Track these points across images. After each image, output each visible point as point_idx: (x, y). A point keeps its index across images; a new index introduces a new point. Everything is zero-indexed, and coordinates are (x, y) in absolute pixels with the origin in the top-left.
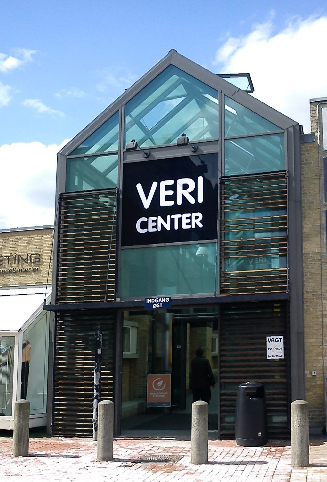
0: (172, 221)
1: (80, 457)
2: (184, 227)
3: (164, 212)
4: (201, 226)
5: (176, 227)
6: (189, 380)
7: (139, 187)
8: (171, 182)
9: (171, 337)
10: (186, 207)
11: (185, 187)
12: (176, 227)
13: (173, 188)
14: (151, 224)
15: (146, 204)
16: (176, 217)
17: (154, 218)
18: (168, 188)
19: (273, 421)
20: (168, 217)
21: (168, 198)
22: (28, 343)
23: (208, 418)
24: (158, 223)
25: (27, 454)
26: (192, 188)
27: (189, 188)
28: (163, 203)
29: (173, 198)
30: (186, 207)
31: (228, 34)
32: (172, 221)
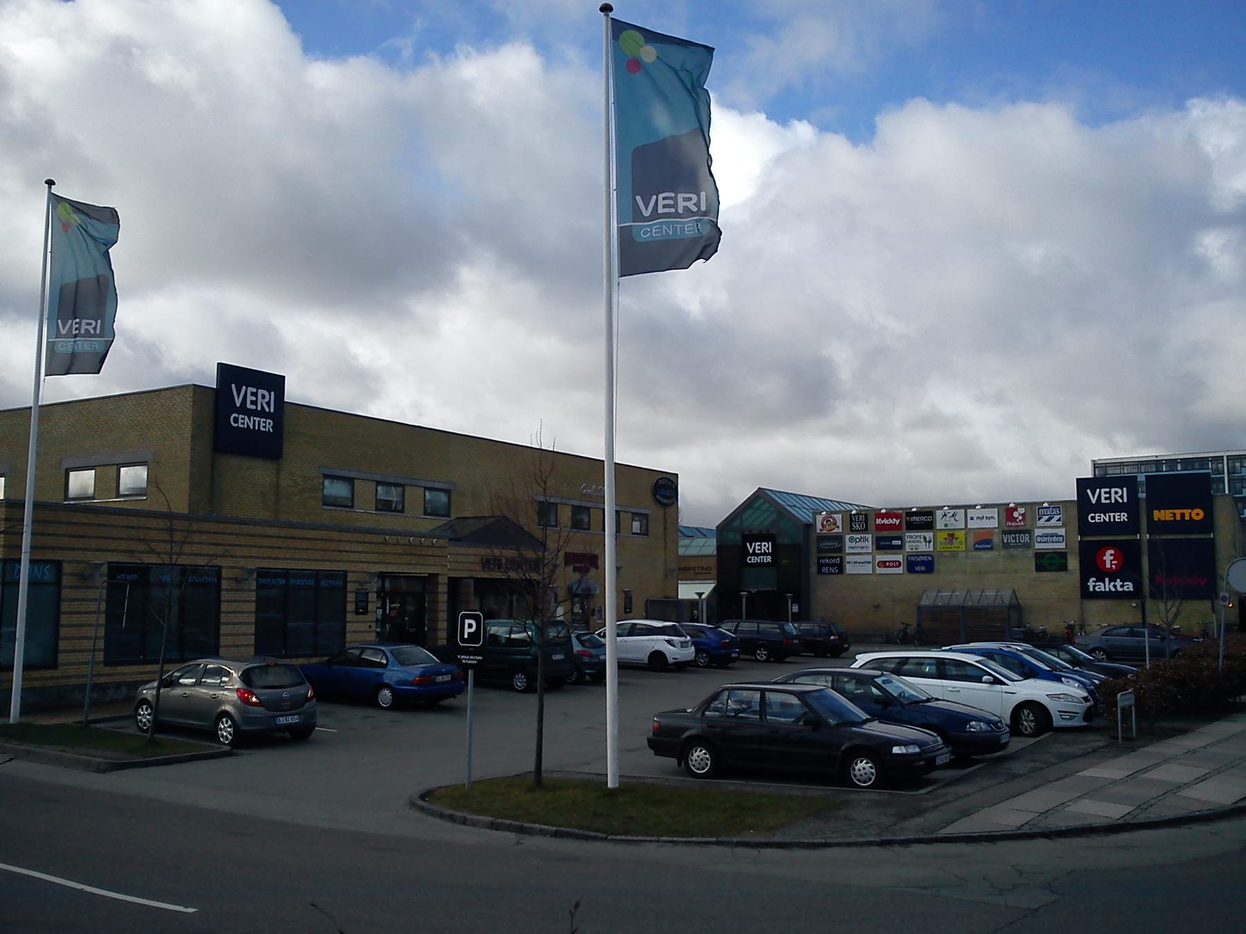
3: (758, 555)
8: (254, 390)
10: (765, 554)
11: (263, 397)
13: (1109, 493)
16: (257, 419)
18: (253, 394)
21: (252, 402)
24: (754, 560)
27: (766, 546)
28: (249, 406)
29: (1109, 498)
30: (765, 554)
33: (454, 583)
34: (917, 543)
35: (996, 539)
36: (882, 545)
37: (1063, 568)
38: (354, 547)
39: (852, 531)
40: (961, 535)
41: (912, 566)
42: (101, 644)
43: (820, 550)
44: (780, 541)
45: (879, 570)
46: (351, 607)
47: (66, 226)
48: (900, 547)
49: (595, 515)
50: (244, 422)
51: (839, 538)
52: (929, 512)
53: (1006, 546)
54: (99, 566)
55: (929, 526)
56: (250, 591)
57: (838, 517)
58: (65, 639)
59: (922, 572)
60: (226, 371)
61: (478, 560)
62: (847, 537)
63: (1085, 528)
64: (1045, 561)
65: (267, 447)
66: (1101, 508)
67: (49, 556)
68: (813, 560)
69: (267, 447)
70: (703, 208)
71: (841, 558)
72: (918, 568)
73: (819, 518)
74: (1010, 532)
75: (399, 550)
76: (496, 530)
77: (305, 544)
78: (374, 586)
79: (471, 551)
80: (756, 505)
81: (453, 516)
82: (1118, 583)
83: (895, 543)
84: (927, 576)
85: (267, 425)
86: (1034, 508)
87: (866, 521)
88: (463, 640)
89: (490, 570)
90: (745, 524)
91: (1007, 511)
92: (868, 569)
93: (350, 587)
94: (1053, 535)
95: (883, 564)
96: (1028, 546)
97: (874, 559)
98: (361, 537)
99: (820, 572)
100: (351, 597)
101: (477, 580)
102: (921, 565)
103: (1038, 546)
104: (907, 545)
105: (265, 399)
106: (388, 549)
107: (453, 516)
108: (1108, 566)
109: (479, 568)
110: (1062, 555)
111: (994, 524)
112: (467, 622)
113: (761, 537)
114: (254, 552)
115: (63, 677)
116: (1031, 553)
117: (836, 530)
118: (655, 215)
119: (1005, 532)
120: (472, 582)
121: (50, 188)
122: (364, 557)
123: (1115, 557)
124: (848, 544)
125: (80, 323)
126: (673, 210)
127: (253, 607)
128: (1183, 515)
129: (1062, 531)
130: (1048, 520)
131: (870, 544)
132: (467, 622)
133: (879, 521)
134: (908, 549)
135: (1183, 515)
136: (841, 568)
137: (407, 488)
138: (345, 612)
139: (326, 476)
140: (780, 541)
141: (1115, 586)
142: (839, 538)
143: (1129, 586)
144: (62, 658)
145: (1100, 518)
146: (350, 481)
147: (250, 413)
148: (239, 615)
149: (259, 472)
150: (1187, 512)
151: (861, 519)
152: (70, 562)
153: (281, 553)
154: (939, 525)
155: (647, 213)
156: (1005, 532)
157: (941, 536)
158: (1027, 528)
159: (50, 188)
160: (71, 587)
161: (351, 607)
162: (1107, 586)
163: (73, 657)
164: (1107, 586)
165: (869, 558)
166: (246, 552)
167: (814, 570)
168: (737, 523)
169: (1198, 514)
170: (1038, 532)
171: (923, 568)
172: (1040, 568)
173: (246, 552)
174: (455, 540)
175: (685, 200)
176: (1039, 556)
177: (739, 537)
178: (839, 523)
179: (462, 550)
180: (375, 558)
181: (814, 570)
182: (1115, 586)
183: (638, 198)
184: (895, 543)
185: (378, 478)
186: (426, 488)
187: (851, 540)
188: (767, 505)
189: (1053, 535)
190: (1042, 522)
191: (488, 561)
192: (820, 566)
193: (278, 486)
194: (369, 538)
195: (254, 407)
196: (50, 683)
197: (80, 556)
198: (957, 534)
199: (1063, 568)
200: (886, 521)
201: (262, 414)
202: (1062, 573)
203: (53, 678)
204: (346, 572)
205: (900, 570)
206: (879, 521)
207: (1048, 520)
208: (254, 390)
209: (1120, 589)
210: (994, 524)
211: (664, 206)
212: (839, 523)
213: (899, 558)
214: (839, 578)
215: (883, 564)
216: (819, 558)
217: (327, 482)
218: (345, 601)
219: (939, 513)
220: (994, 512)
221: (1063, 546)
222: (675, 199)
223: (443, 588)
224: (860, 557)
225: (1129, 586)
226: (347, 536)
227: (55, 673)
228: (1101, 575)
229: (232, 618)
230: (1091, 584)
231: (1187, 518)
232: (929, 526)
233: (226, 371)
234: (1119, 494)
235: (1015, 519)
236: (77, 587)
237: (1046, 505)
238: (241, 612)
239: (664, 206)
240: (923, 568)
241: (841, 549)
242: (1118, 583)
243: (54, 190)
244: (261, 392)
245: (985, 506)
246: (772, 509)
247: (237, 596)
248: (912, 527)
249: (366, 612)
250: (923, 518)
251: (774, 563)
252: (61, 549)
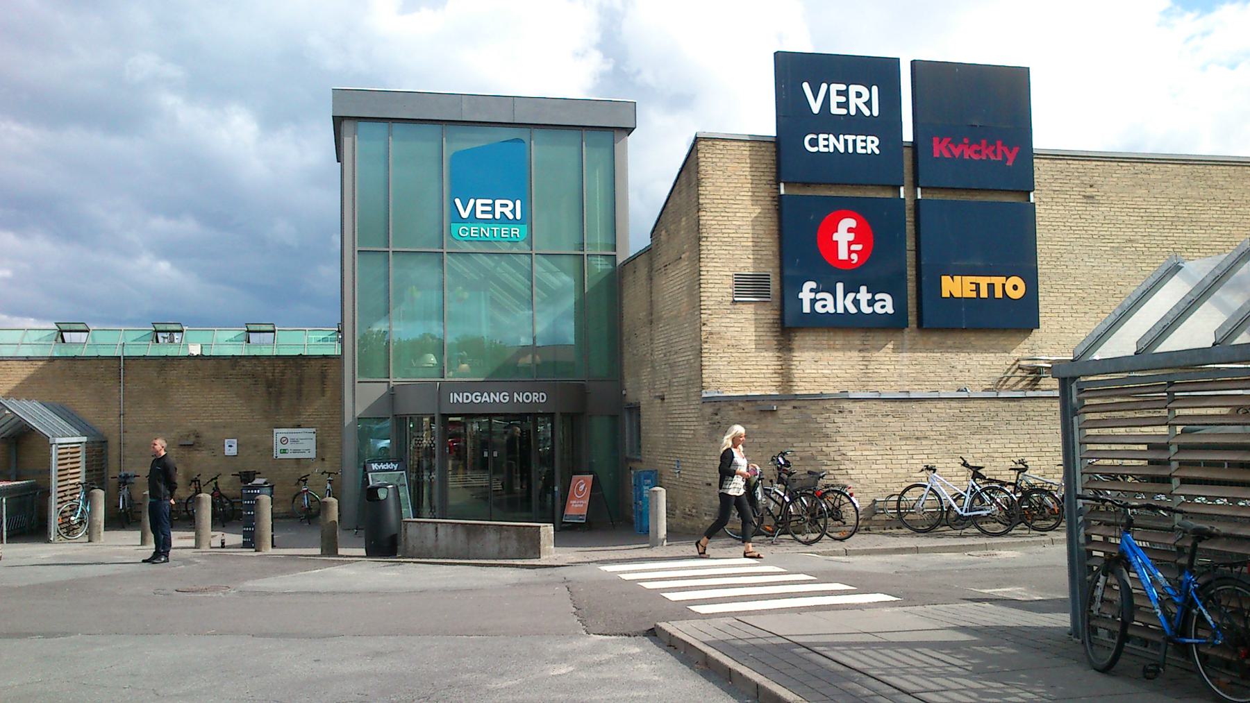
0: (846, 141)
2: (860, 151)
4: (877, 152)
5: (850, 150)
7: (806, 86)
11: (859, 95)
12: (850, 150)
13: (844, 93)
14: (822, 143)
15: (816, 107)
16: (850, 138)
17: (826, 136)
18: (839, 93)
19: (1056, 479)
20: (841, 137)
21: (839, 105)
22: (935, 471)
25: (335, 554)
28: (479, 215)
29: (845, 105)
31: (890, 346)
32: (846, 141)
49: (525, 515)
60: (795, 71)
66: (829, 123)
70: (518, 216)
82: (864, 295)
108: (843, 254)
118: (473, 217)
123: (859, 234)
126: (490, 216)
128: (991, 287)
135: (991, 287)
141: (856, 302)
143: (885, 304)
145: (828, 143)
150: (998, 281)
155: (465, 215)
162: (838, 302)
164: (838, 302)
169: (1014, 287)
175: (502, 205)
182: (856, 302)
183: (457, 201)
209: (866, 310)
211: (483, 212)
222: (493, 206)
225: (885, 304)
228: (831, 274)
230: (806, 295)
231: (998, 294)
233: (795, 71)
234: (862, 99)
239: (483, 212)
242: (864, 295)
244: (853, 89)
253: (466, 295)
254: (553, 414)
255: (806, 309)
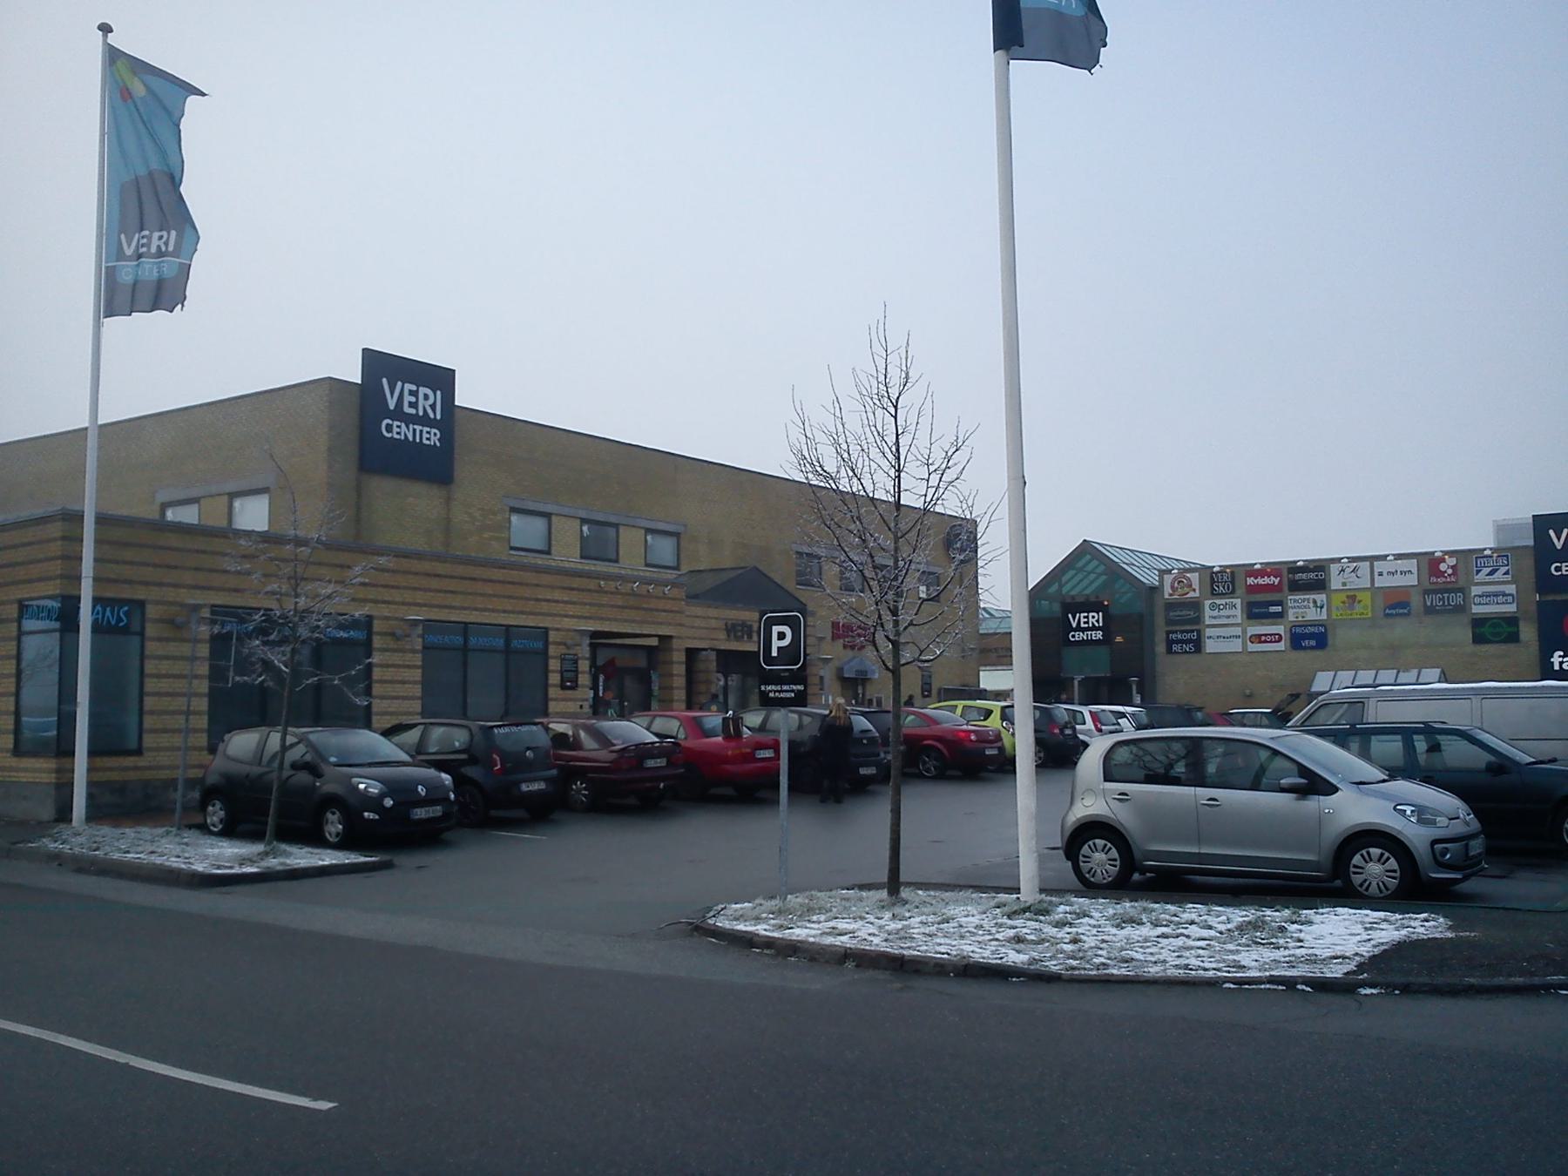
1: (204, 94)
3: (1083, 630)
6: (122, 1061)
7: (1552, 533)
8: (414, 388)
9: (224, 889)
10: (1094, 628)
11: (426, 397)
14: (395, 430)
16: (418, 428)
18: (411, 393)
21: (411, 405)
23: (1346, 910)
24: (1079, 636)
26: (431, 401)
27: (1095, 618)
28: (407, 410)
30: (1094, 628)
33: (691, 654)
34: (1304, 609)
35: (1416, 601)
36: (1256, 612)
37: (1514, 638)
38: (557, 595)
39: (1214, 594)
40: (1366, 598)
41: (1297, 641)
42: (203, 704)
43: (1169, 622)
44: (1113, 611)
45: (1252, 647)
46: (554, 678)
47: (126, 94)
48: (1280, 615)
50: (399, 431)
51: (1196, 605)
52: (1320, 567)
53: (1430, 611)
54: (196, 608)
55: (1320, 585)
56: (414, 651)
57: (1194, 577)
58: (152, 713)
59: (1312, 648)
60: (374, 361)
61: (721, 624)
62: (1207, 603)
63: (1545, 582)
64: (1486, 630)
65: (432, 466)
67: (127, 593)
68: (1160, 637)
69: (432, 466)
71: (1199, 632)
72: (1306, 643)
73: (1168, 579)
74: (1435, 592)
75: (619, 601)
76: (748, 587)
77: (488, 589)
78: (584, 651)
79: (712, 612)
80: (1080, 564)
81: (685, 569)
83: (1273, 609)
84: (1319, 653)
85: (432, 437)
86: (1468, 558)
87: (1233, 582)
88: (769, 660)
89: (738, 639)
90: (1064, 590)
91: (1431, 563)
92: (1236, 646)
93: (552, 650)
94: (1496, 595)
95: (1258, 638)
96: (1461, 609)
97: (1244, 632)
98: (568, 582)
99: (1169, 651)
100: (554, 664)
101: (719, 652)
102: (1310, 639)
103: (1475, 609)
104: (1291, 612)
105: (428, 400)
106: (605, 600)
107: (685, 569)
109: (723, 635)
110: (1512, 620)
111: (1412, 580)
112: (776, 629)
113: (1088, 606)
114: (420, 597)
115: (149, 768)
116: (1466, 620)
117: (1192, 594)
119: (1427, 592)
120: (713, 656)
121: (105, 36)
122: (571, 610)
124: (1208, 612)
125: (149, 238)
127: (417, 690)
129: (1511, 589)
130: (1491, 573)
131: (1238, 612)
132: (776, 629)
133: (1250, 581)
134: (1291, 618)
136: (1198, 646)
137: (622, 529)
138: (546, 686)
139: (514, 510)
140: (1113, 611)
142: (1196, 605)
144: (148, 740)
146: (547, 516)
147: (409, 420)
148: (398, 680)
149: (421, 500)
151: (1222, 581)
152: (157, 603)
153: (457, 601)
154: (1335, 583)
156: (1427, 592)
157: (1337, 600)
158: (1461, 584)
159: (105, 36)
160: (160, 639)
161: (554, 678)
163: (165, 740)
165: (1238, 631)
166: (408, 596)
167: (1161, 648)
168: (1053, 589)
170: (1475, 590)
171: (1313, 643)
172: (1478, 639)
173: (408, 596)
174: (693, 597)
176: (1478, 623)
177: (1057, 607)
178: (1196, 585)
179: (699, 611)
180: (585, 611)
181: (1161, 648)
184: (1273, 609)
185: (583, 514)
186: (649, 531)
187: (1213, 607)
188: (1095, 563)
189: (1496, 595)
190: (1481, 577)
191: (734, 625)
192: (1170, 643)
193: (448, 520)
194: (576, 582)
195: (413, 411)
196: (132, 776)
197: (170, 594)
198: (1360, 596)
199: (1514, 638)
200: (1260, 581)
201: (425, 420)
202: (1512, 646)
203: (137, 768)
204: (546, 630)
205: (1281, 646)
206: (1250, 581)
207: (1491, 573)
208: (414, 388)
210: (1412, 580)
212: (1196, 585)
213: (1280, 629)
214: (1195, 658)
215: (1258, 638)
216: (1168, 633)
217: (514, 518)
218: (546, 671)
219: (1334, 568)
220: (1412, 565)
221: (1512, 608)
223: (679, 657)
224: (1226, 630)
226: (546, 579)
227: (141, 762)
229: (389, 690)
232: (1320, 585)
233: (374, 361)
235: (1441, 580)
236: (167, 640)
237: (1488, 552)
238: (403, 682)
240: (1313, 643)
241: (1198, 620)
243: (112, 39)
244: (423, 390)
245: (1399, 557)
246: (1102, 568)
247: (396, 658)
248: (1296, 587)
249: (574, 687)
250: (1312, 575)
251: (1107, 640)
252: (147, 584)
253: (526, 531)
254: (548, 553)
255: (1557, 667)
